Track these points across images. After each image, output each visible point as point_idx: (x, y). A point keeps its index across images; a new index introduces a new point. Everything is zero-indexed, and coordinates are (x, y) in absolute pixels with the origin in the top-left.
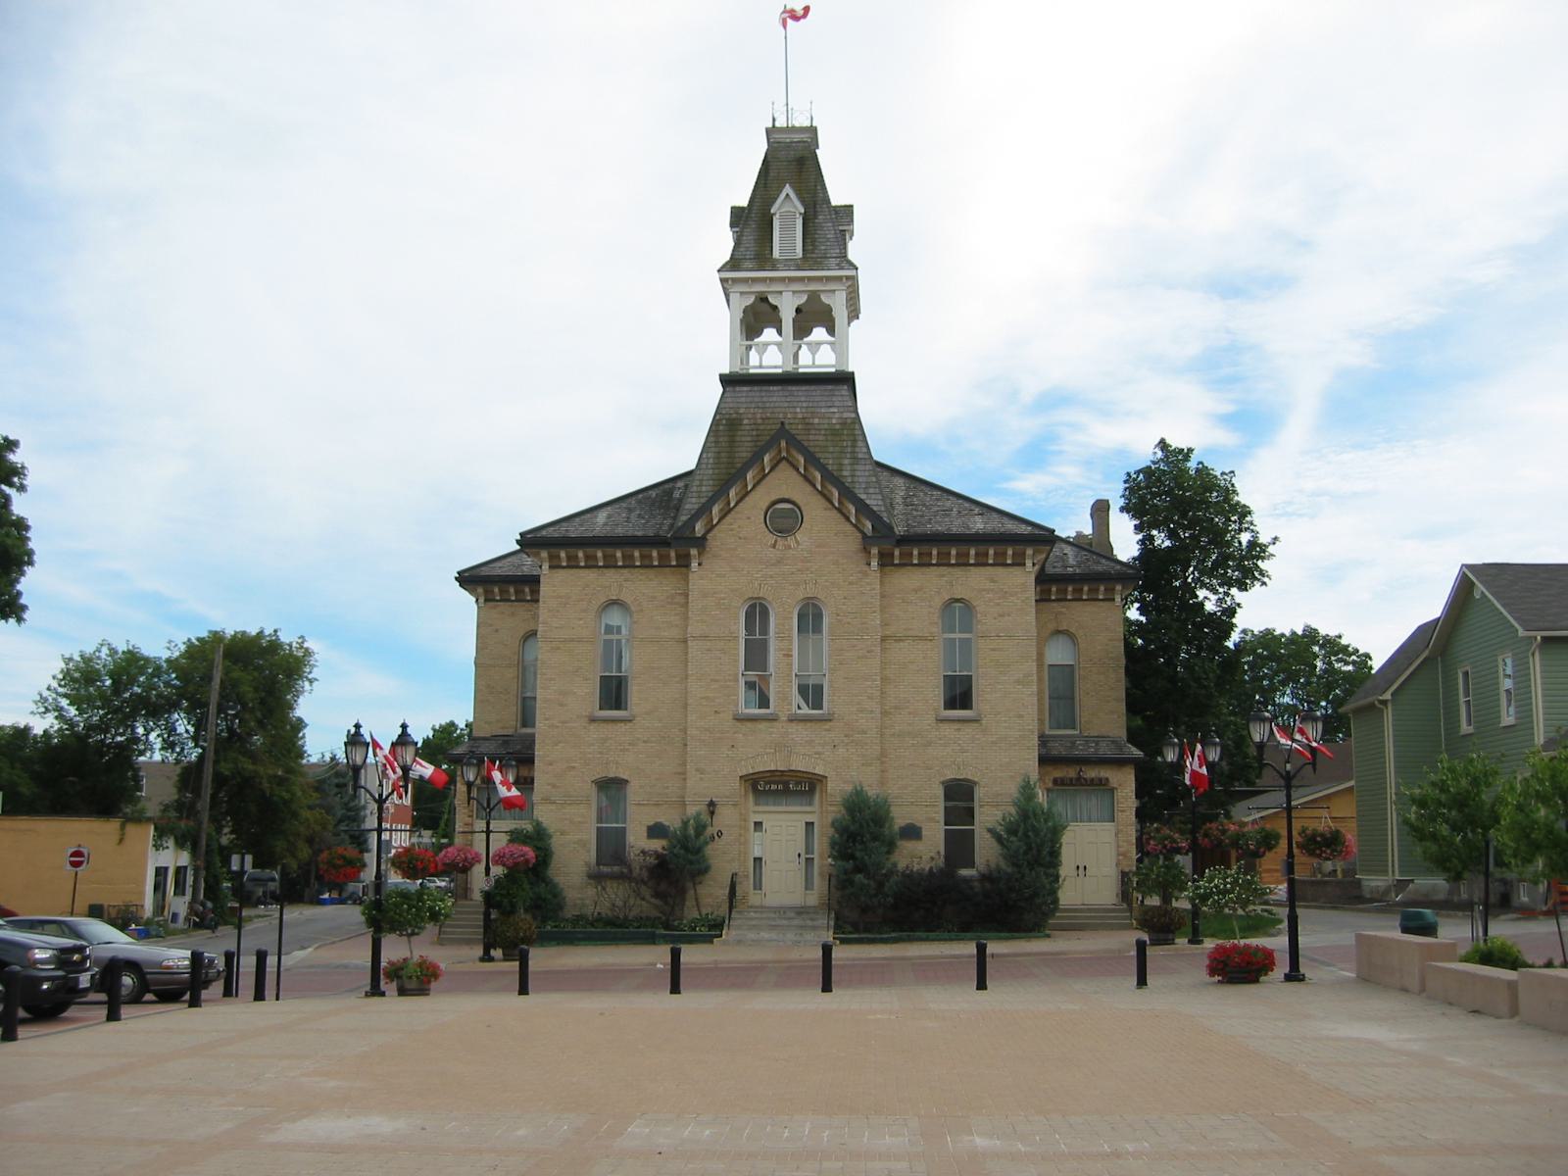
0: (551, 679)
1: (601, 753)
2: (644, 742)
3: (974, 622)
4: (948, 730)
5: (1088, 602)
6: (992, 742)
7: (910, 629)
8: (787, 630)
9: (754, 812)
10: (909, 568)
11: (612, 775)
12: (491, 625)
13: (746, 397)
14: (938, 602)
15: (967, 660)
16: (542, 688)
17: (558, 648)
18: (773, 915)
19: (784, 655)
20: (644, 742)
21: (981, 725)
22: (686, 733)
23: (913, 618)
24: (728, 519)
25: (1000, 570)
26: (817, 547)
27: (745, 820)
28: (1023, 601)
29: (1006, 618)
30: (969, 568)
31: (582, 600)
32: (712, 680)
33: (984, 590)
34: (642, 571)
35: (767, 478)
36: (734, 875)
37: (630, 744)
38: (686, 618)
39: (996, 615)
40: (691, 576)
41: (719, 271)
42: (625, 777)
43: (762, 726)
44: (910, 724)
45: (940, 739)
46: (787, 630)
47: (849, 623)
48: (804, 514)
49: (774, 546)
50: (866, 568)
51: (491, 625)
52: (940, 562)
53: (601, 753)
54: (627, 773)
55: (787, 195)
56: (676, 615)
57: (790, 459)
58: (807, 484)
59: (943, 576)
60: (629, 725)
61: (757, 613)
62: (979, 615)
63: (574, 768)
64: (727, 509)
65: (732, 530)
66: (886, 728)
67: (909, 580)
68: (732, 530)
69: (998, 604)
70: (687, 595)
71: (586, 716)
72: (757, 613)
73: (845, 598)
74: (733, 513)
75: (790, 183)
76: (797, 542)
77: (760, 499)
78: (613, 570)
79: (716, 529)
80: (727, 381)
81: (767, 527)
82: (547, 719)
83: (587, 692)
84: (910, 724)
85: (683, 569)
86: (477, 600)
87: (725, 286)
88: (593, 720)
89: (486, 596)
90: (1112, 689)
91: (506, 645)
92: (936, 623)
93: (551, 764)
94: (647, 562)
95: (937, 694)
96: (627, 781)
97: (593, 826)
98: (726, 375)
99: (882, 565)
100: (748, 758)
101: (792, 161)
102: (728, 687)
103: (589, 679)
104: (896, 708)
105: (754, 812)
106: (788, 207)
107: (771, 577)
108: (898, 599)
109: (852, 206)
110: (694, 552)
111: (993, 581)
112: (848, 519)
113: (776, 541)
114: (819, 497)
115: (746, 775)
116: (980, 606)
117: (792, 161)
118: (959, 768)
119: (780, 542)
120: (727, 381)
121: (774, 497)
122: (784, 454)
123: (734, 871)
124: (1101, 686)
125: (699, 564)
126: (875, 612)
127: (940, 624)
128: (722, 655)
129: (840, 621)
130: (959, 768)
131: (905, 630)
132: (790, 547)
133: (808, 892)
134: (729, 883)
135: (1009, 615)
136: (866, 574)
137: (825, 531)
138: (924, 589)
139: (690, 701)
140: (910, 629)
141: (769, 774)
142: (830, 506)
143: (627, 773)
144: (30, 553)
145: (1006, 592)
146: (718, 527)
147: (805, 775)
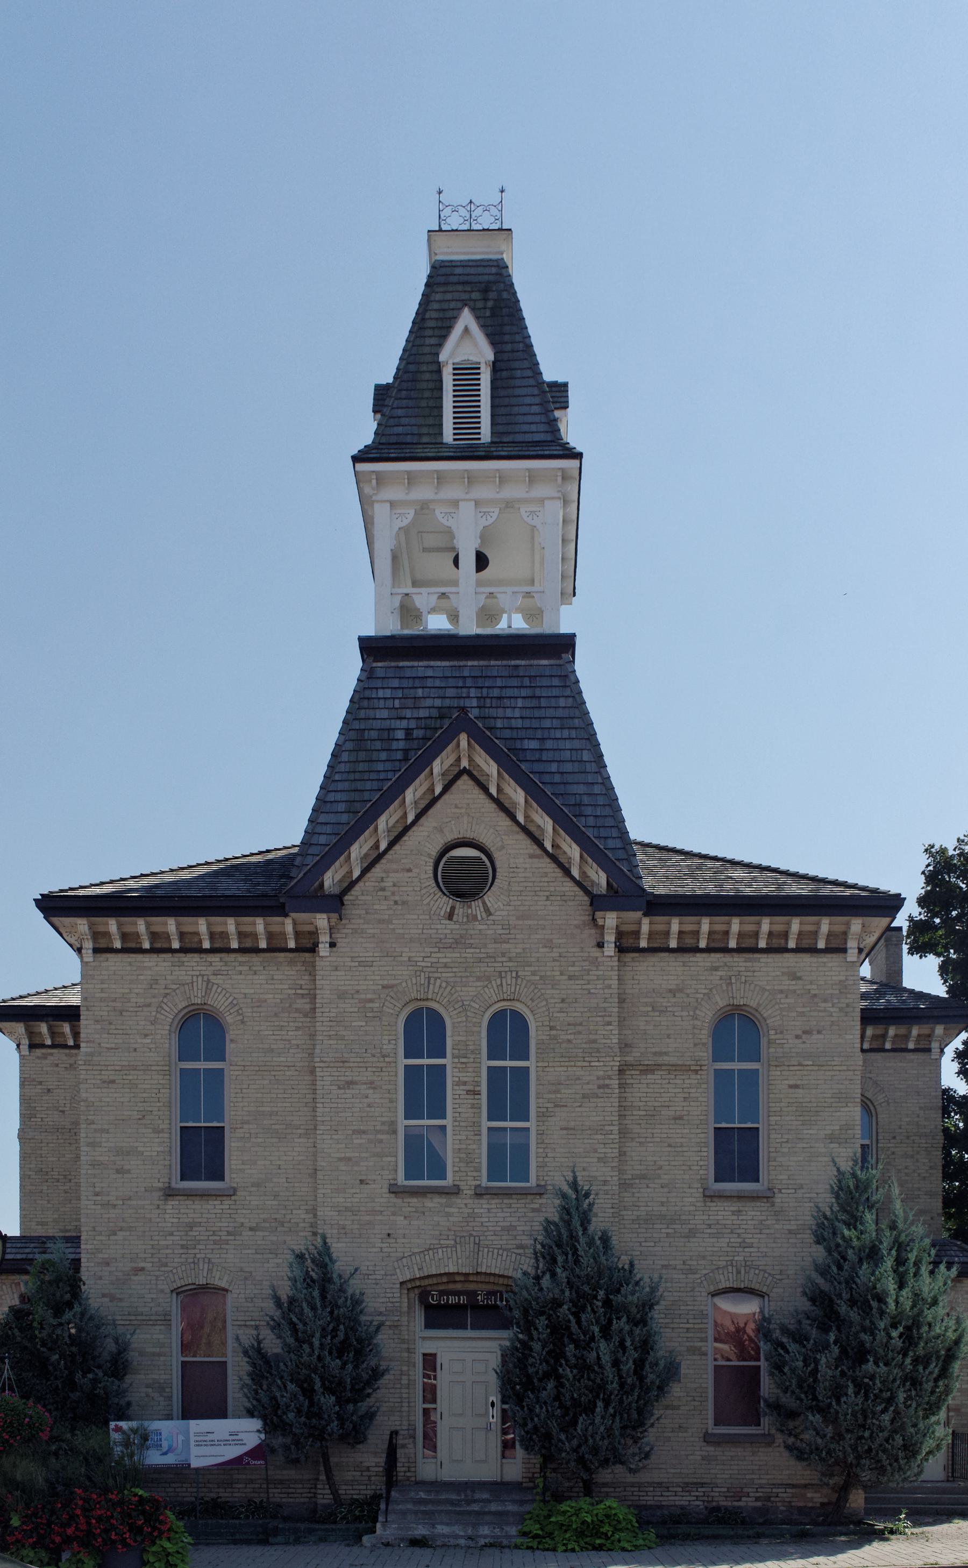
0: (103, 1131)
1: (183, 1247)
2: (251, 1229)
3: (764, 1041)
4: (723, 1212)
5: (891, 1054)
6: (790, 1232)
7: (666, 1054)
8: (473, 1052)
9: (424, 1338)
10: (663, 955)
11: (202, 1281)
12: (40, 1083)
13: (420, 435)
14: (708, 1014)
15: (751, 1106)
16: (88, 1145)
17: (113, 1082)
18: (454, 1497)
19: (468, 1092)
20: (251, 1229)
21: (773, 1205)
22: (315, 1216)
23: (669, 1036)
24: (377, 871)
25: (806, 960)
26: (518, 919)
27: (408, 1350)
28: (841, 1009)
29: (816, 1037)
30: (757, 956)
31: (149, 1005)
32: (354, 1132)
33: (781, 992)
34: (241, 958)
35: (438, 805)
36: (394, 1434)
37: (229, 1233)
38: (312, 1036)
39: (799, 1033)
40: (319, 963)
41: (356, 459)
42: (223, 1284)
43: (433, 1203)
44: (662, 1204)
45: (710, 1226)
46: (473, 1052)
47: (569, 1041)
48: (498, 864)
49: (450, 916)
50: (595, 952)
51: (40, 1083)
52: (713, 945)
53: (183, 1247)
54: (226, 1278)
55: (466, 330)
56: (298, 1029)
57: (475, 773)
58: (502, 815)
59: (716, 969)
60: (227, 1202)
61: (424, 1031)
62: (772, 1032)
63: (143, 1269)
64: (374, 855)
65: (383, 889)
66: (625, 1208)
67: (657, 974)
68: (383, 889)
69: (802, 1014)
70: (314, 997)
71: (160, 1189)
72: (424, 1031)
73: (563, 1001)
74: (383, 861)
75: (473, 310)
76: (488, 911)
77: (426, 840)
78: (196, 957)
79: (357, 887)
80: (371, 648)
81: (441, 890)
82: (97, 1194)
83: (158, 1151)
84: (662, 1204)
85: (307, 955)
86: (18, 1046)
87: (367, 490)
88: (170, 1193)
89: (30, 1039)
90: (924, 1178)
91: (63, 1112)
92: (704, 1044)
93: (108, 1264)
94: (248, 944)
95: (701, 1157)
96: (227, 1290)
97: (176, 1359)
98: (369, 639)
99: (621, 949)
100: (414, 1254)
101: (472, 286)
102: (381, 1141)
103: (162, 1131)
104: (643, 1177)
105: (424, 1338)
106: (467, 344)
107: (446, 966)
108: (646, 1005)
109: (565, 385)
110: (322, 921)
111: (795, 977)
112: (567, 872)
113: (453, 908)
114: (522, 836)
115: (410, 1280)
116: (771, 1016)
117: (472, 286)
118: (739, 1272)
119: (460, 911)
120: (371, 648)
121: (450, 837)
122: (465, 763)
123: (393, 1428)
124: (907, 1175)
125: (332, 945)
126: (609, 1024)
127: (710, 1045)
128: (371, 1091)
129: (555, 1038)
130: (739, 1272)
131: (655, 1054)
132: (475, 918)
133: (504, 1461)
134: (386, 1446)
135: (819, 1032)
136: (595, 962)
137: (533, 889)
138: (683, 991)
139: (321, 1163)
140: (666, 1054)
141: (445, 1279)
142: (539, 852)
143: (226, 1278)
144: (365, 1439)
145: (815, 996)
146: (361, 884)
147: (501, 1281)
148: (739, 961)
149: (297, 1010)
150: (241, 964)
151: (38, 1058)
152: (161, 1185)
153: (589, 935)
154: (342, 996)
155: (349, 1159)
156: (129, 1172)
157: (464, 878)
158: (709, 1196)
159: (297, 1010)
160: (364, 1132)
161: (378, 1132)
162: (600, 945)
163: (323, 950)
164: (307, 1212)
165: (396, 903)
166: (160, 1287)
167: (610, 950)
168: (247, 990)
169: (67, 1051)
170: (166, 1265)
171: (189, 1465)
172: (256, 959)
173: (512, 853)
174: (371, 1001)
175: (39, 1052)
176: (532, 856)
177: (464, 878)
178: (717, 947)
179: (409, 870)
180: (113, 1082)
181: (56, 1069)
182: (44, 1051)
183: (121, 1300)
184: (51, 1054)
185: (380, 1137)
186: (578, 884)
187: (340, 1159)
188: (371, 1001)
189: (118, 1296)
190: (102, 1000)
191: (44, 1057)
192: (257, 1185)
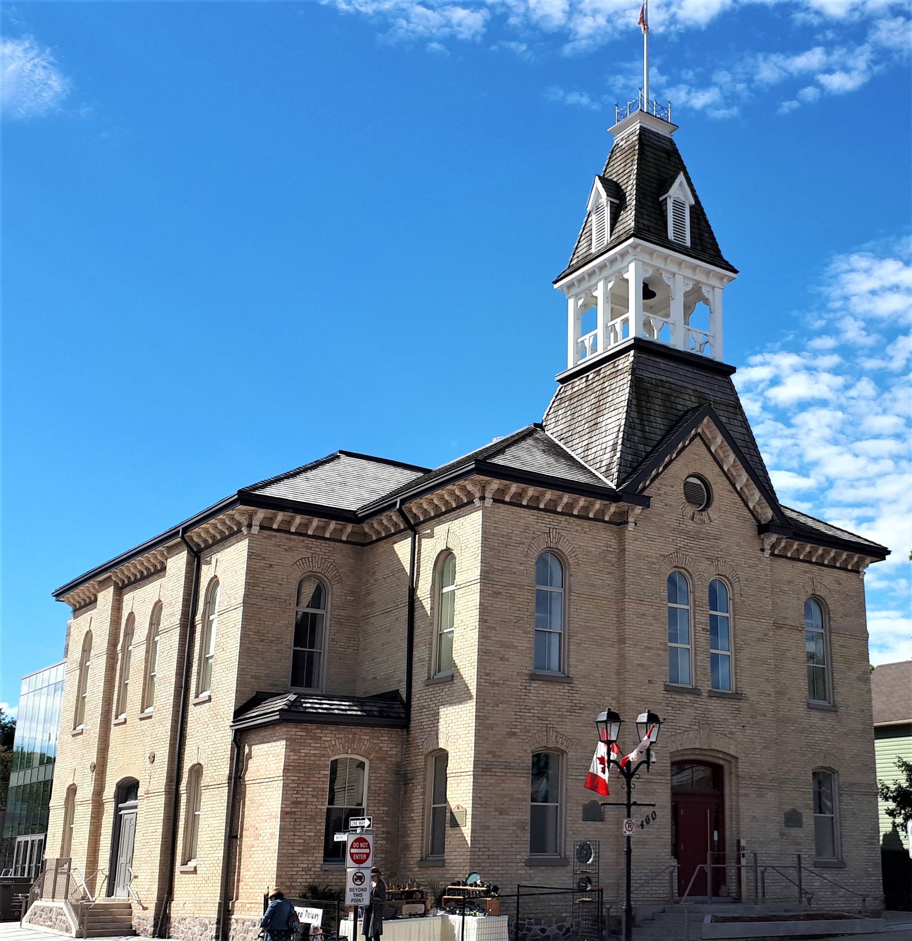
31: (523, 544)
34: (579, 522)
51: (264, 559)
56: (609, 573)
67: (787, 570)
68: (660, 495)
71: (527, 675)
114: (724, 478)
148: (815, 568)
149: (608, 561)
150: (578, 525)
151: (264, 538)
152: (527, 672)
153: (756, 543)
154: (639, 557)
155: (643, 665)
156: (507, 660)
157: (699, 495)
158: (810, 707)
159: (608, 561)
160: (651, 648)
161: (659, 649)
162: (762, 550)
163: (631, 526)
164: (613, 699)
165: (666, 505)
166: (525, 748)
167: (767, 553)
168: (583, 541)
169: (288, 536)
170: (528, 731)
171: (58, 860)
172: (586, 523)
173: (719, 487)
174: (654, 563)
175: (266, 533)
176: (729, 491)
177: (699, 495)
178: (550, 509)
179: (672, 486)
180: (500, 593)
181: (278, 549)
182: (270, 533)
183: (499, 756)
184: (275, 537)
185: (660, 652)
186: (751, 512)
187: (639, 665)
188: (654, 563)
189: (498, 753)
190: (494, 535)
191: (269, 538)
192: (584, 677)
